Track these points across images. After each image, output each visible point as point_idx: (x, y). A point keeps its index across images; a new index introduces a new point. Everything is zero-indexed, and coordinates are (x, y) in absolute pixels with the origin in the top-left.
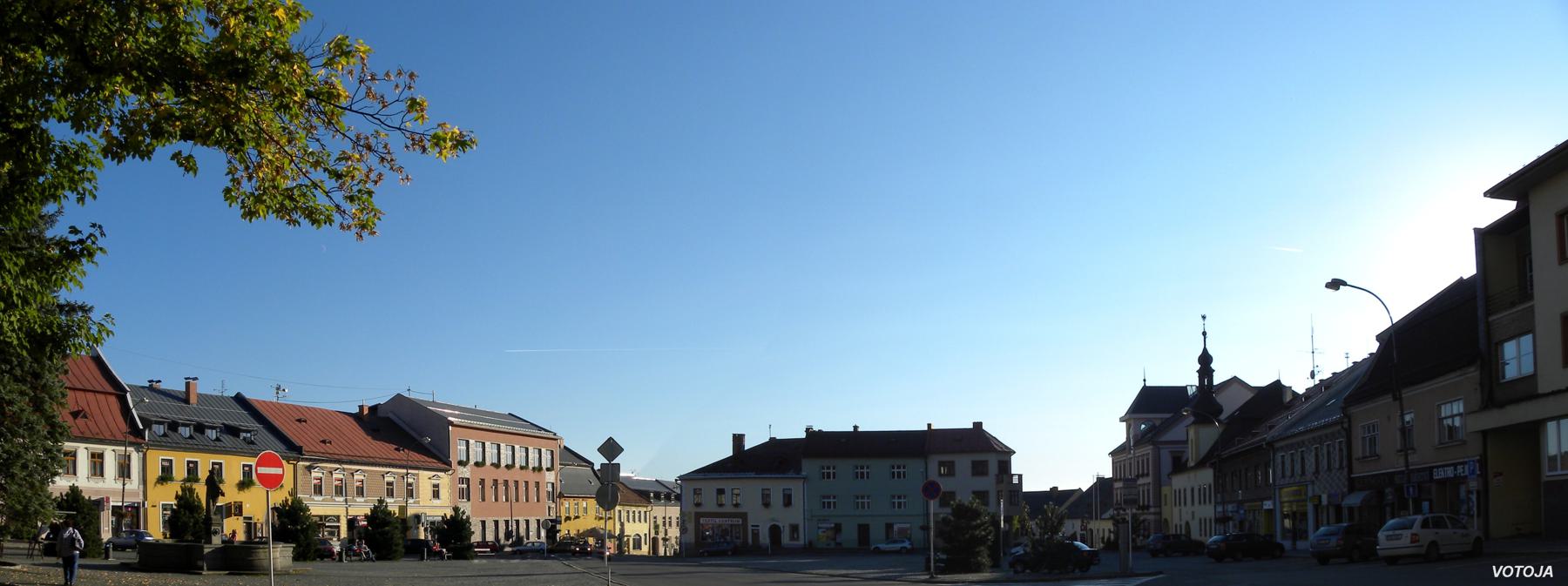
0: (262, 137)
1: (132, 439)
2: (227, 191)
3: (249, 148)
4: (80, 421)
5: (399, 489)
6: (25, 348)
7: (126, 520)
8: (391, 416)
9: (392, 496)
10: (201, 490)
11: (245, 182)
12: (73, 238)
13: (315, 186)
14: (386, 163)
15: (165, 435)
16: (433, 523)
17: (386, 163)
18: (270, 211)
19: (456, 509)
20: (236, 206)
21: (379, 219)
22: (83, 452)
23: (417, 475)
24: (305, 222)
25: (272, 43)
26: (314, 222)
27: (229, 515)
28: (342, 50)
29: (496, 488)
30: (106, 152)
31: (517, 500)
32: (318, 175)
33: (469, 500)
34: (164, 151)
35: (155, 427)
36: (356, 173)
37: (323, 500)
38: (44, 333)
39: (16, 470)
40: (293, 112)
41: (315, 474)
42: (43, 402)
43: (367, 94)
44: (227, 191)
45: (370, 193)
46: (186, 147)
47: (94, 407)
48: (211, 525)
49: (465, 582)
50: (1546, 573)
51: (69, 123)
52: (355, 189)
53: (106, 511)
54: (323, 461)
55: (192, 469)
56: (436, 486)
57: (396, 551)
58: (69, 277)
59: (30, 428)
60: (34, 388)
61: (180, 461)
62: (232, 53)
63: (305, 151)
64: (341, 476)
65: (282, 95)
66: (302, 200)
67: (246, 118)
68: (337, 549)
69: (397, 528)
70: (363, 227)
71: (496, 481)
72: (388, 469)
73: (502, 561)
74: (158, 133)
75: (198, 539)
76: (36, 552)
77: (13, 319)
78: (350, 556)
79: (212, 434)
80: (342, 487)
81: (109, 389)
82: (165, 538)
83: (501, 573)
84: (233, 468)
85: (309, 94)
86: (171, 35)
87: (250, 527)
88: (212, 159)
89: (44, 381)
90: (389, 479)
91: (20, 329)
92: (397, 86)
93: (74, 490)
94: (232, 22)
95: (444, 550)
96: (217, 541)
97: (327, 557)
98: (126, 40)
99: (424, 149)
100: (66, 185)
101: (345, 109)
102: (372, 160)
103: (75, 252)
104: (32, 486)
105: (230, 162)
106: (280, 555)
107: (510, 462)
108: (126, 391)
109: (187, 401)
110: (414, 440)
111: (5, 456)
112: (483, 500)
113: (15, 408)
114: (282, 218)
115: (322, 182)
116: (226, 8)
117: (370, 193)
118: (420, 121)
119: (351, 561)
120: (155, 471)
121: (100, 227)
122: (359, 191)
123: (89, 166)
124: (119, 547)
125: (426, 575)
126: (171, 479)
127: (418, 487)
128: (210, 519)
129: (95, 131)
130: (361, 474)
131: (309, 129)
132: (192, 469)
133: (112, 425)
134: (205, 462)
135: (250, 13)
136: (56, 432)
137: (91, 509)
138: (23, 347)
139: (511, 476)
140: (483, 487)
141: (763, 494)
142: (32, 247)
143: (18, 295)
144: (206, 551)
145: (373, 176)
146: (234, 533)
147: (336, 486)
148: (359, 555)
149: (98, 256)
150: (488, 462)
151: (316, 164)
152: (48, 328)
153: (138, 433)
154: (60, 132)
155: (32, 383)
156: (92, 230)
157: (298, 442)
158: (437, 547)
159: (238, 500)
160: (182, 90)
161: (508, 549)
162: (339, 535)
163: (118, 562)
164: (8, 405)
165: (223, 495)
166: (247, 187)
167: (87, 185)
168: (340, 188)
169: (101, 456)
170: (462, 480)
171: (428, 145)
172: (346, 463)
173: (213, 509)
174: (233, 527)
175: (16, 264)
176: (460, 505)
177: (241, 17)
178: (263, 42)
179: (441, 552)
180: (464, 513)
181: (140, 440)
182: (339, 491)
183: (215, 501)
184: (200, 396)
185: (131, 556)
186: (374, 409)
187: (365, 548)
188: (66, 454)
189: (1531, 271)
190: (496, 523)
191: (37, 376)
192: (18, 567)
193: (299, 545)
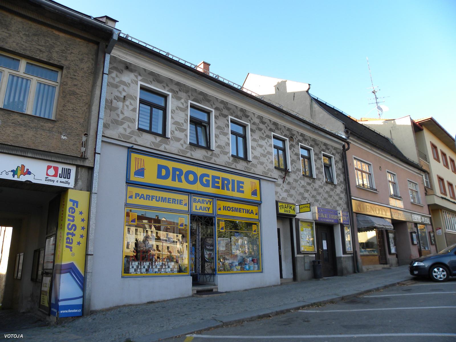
50: (21, 336)
189: (90, 17)
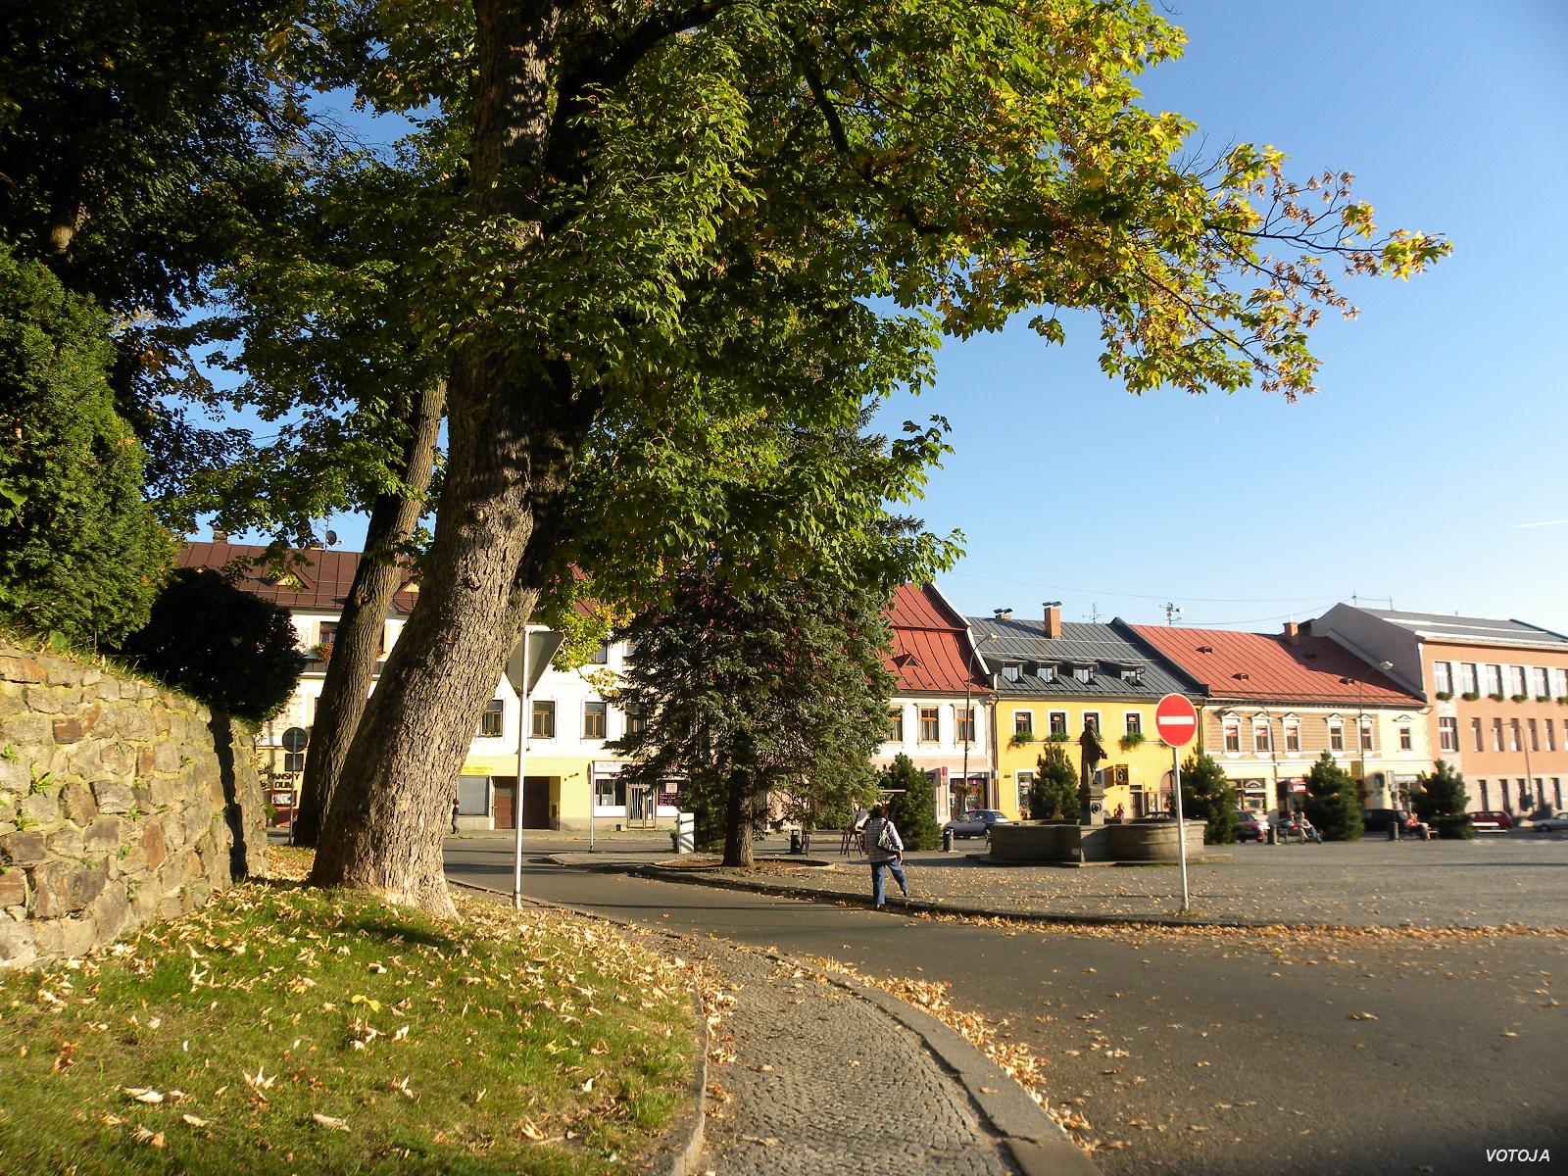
0: (1146, 283)
1: (976, 688)
2: (1105, 359)
3: (1133, 305)
4: (906, 669)
5: (1351, 736)
6: (853, 579)
7: (971, 797)
8: (1331, 635)
9: (1340, 747)
10: (1074, 753)
11: (1127, 345)
12: (910, 436)
13: (1223, 338)
14: (1320, 296)
15: (1020, 681)
16: (1403, 785)
17: (1320, 296)
18: (1165, 378)
19: (1439, 764)
20: (1119, 376)
21: (1315, 370)
22: (910, 709)
23: (1375, 716)
24: (1213, 387)
25: (1154, 170)
26: (1224, 385)
27: (1109, 784)
28: (1246, 162)
29: (1500, 731)
30: (947, 327)
31: (1536, 748)
32: (1227, 324)
33: (1457, 749)
34: (1018, 319)
35: (1006, 671)
36: (1279, 315)
37: (1241, 758)
38: (874, 559)
39: (828, 738)
40: (1190, 250)
41: (1228, 721)
42: (861, 649)
43: (1287, 211)
44: (1105, 359)
45: (1301, 339)
46: (1047, 311)
47: (926, 654)
48: (1089, 798)
49: (1466, 874)
51: (892, 297)
52: (1280, 335)
53: (943, 787)
54: (1238, 703)
55: (1058, 723)
56: (1405, 731)
57: (1351, 828)
58: (906, 485)
59: (846, 681)
60: (849, 630)
61: (1041, 714)
62: (1103, 189)
63: (1205, 296)
64: (1265, 723)
65: (1174, 231)
66: (1207, 358)
67: (1127, 266)
68: (1264, 826)
69: (1351, 794)
70: (1295, 384)
71: (1498, 722)
72: (1331, 710)
73: (1520, 842)
74: (1014, 298)
75: (1071, 819)
76: (851, 846)
77: (834, 543)
78: (1284, 836)
79: (1083, 675)
80: (1266, 738)
81: (945, 625)
82: (1025, 819)
83: (1523, 861)
84: (1112, 720)
85: (1207, 225)
86: (1021, 176)
87: (1139, 798)
88: (1083, 323)
89: (863, 619)
90: (1333, 723)
91: (844, 556)
92: (1326, 194)
93: (902, 761)
94: (1095, 151)
95: (1425, 825)
96: (1097, 820)
97: (1251, 837)
98: (969, 192)
99: (1374, 270)
100: (896, 371)
101: (1257, 235)
102: (1301, 294)
103: (914, 452)
104: (849, 758)
105: (1105, 322)
106: (1188, 836)
107: (1519, 692)
108: (966, 627)
109: (1047, 634)
110: (1369, 666)
111: (813, 720)
112: (1480, 749)
113: (827, 658)
114: (1182, 385)
115: (1231, 332)
116: (1085, 135)
117: (1301, 339)
118: (1365, 233)
119: (1286, 843)
120: (1007, 729)
121: (943, 419)
122: (1286, 338)
123: (922, 346)
124: (963, 835)
125: (1402, 862)
126: (1030, 739)
127: (1377, 734)
128: (1088, 791)
129: (929, 304)
130: (1293, 719)
131: (1210, 267)
132: (1058, 723)
133: (950, 673)
134: (1075, 715)
135: (1118, 138)
136: (879, 685)
137: (925, 785)
138: (849, 578)
139: (1522, 712)
140: (1478, 731)
141: (54, 729)
142: (842, 451)
143: (842, 513)
144: (1084, 834)
145: (1304, 316)
146: (1120, 812)
147: (1228, 738)
148: (1298, 833)
149: (943, 456)
150: (1483, 693)
151: (1224, 311)
152: (880, 552)
153: (982, 680)
154: (883, 308)
155: (846, 624)
156: (933, 425)
157: (1201, 679)
158: (1413, 820)
159: (1122, 762)
160: (1040, 242)
161: (1526, 824)
162: (1265, 806)
163: (963, 854)
164: (816, 654)
165: (1105, 757)
166: (1131, 350)
167: (922, 369)
168: (1258, 337)
169: (935, 713)
170: (1444, 721)
171: (1378, 262)
172: (1271, 704)
173: (1091, 777)
174: (1115, 801)
175: (838, 475)
176: (1443, 758)
177: (1106, 144)
178: (1141, 169)
179: (1420, 828)
180: (1451, 769)
181: (986, 690)
182: (1263, 743)
183: (1093, 767)
184: (1064, 625)
185: (980, 846)
186: (1305, 627)
187: (1306, 824)
188: (893, 714)
190: (1504, 783)
191: (852, 614)
192: (830, 868)
193: (1211, 823)
